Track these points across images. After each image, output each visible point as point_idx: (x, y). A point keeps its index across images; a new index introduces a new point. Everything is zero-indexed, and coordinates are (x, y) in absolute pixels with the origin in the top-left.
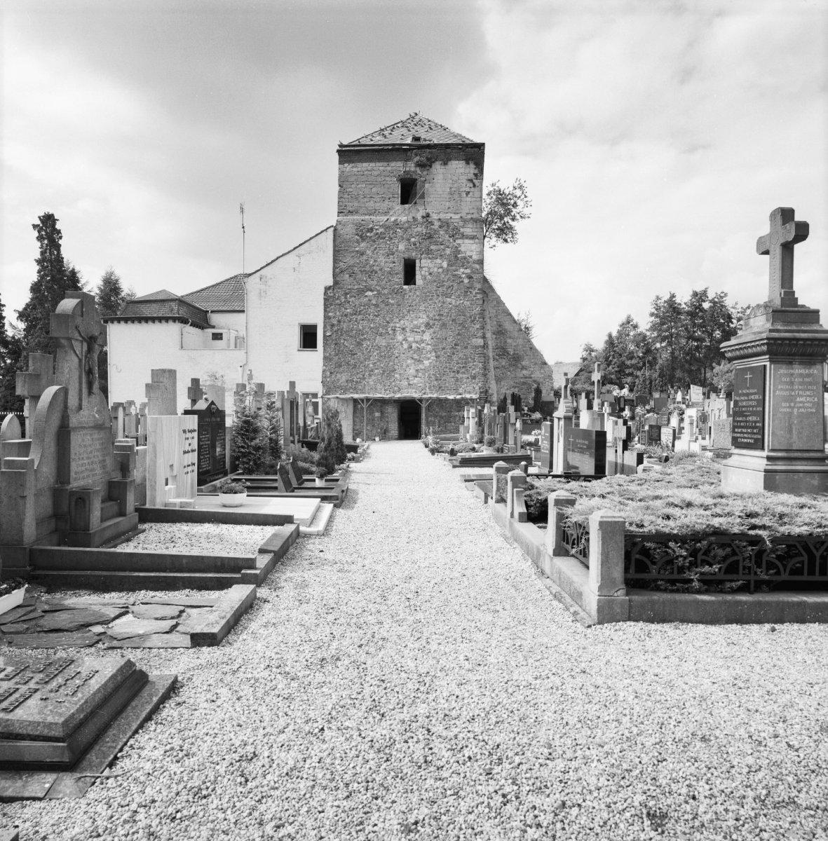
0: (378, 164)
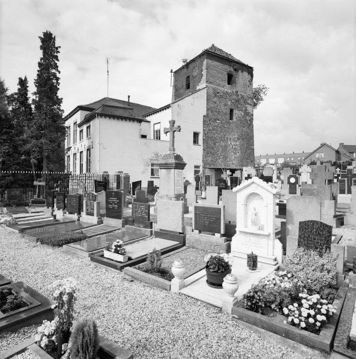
0: (220, 64)
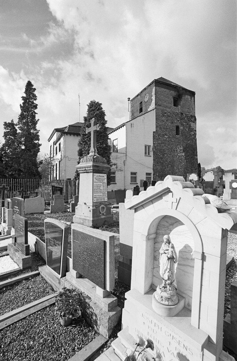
0: (167, 90)
